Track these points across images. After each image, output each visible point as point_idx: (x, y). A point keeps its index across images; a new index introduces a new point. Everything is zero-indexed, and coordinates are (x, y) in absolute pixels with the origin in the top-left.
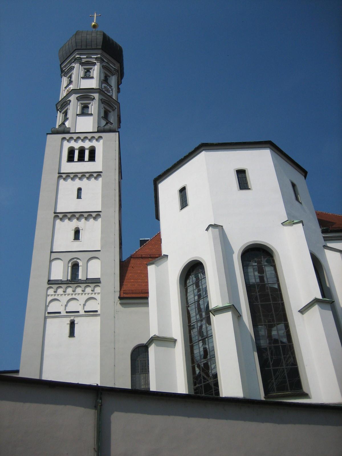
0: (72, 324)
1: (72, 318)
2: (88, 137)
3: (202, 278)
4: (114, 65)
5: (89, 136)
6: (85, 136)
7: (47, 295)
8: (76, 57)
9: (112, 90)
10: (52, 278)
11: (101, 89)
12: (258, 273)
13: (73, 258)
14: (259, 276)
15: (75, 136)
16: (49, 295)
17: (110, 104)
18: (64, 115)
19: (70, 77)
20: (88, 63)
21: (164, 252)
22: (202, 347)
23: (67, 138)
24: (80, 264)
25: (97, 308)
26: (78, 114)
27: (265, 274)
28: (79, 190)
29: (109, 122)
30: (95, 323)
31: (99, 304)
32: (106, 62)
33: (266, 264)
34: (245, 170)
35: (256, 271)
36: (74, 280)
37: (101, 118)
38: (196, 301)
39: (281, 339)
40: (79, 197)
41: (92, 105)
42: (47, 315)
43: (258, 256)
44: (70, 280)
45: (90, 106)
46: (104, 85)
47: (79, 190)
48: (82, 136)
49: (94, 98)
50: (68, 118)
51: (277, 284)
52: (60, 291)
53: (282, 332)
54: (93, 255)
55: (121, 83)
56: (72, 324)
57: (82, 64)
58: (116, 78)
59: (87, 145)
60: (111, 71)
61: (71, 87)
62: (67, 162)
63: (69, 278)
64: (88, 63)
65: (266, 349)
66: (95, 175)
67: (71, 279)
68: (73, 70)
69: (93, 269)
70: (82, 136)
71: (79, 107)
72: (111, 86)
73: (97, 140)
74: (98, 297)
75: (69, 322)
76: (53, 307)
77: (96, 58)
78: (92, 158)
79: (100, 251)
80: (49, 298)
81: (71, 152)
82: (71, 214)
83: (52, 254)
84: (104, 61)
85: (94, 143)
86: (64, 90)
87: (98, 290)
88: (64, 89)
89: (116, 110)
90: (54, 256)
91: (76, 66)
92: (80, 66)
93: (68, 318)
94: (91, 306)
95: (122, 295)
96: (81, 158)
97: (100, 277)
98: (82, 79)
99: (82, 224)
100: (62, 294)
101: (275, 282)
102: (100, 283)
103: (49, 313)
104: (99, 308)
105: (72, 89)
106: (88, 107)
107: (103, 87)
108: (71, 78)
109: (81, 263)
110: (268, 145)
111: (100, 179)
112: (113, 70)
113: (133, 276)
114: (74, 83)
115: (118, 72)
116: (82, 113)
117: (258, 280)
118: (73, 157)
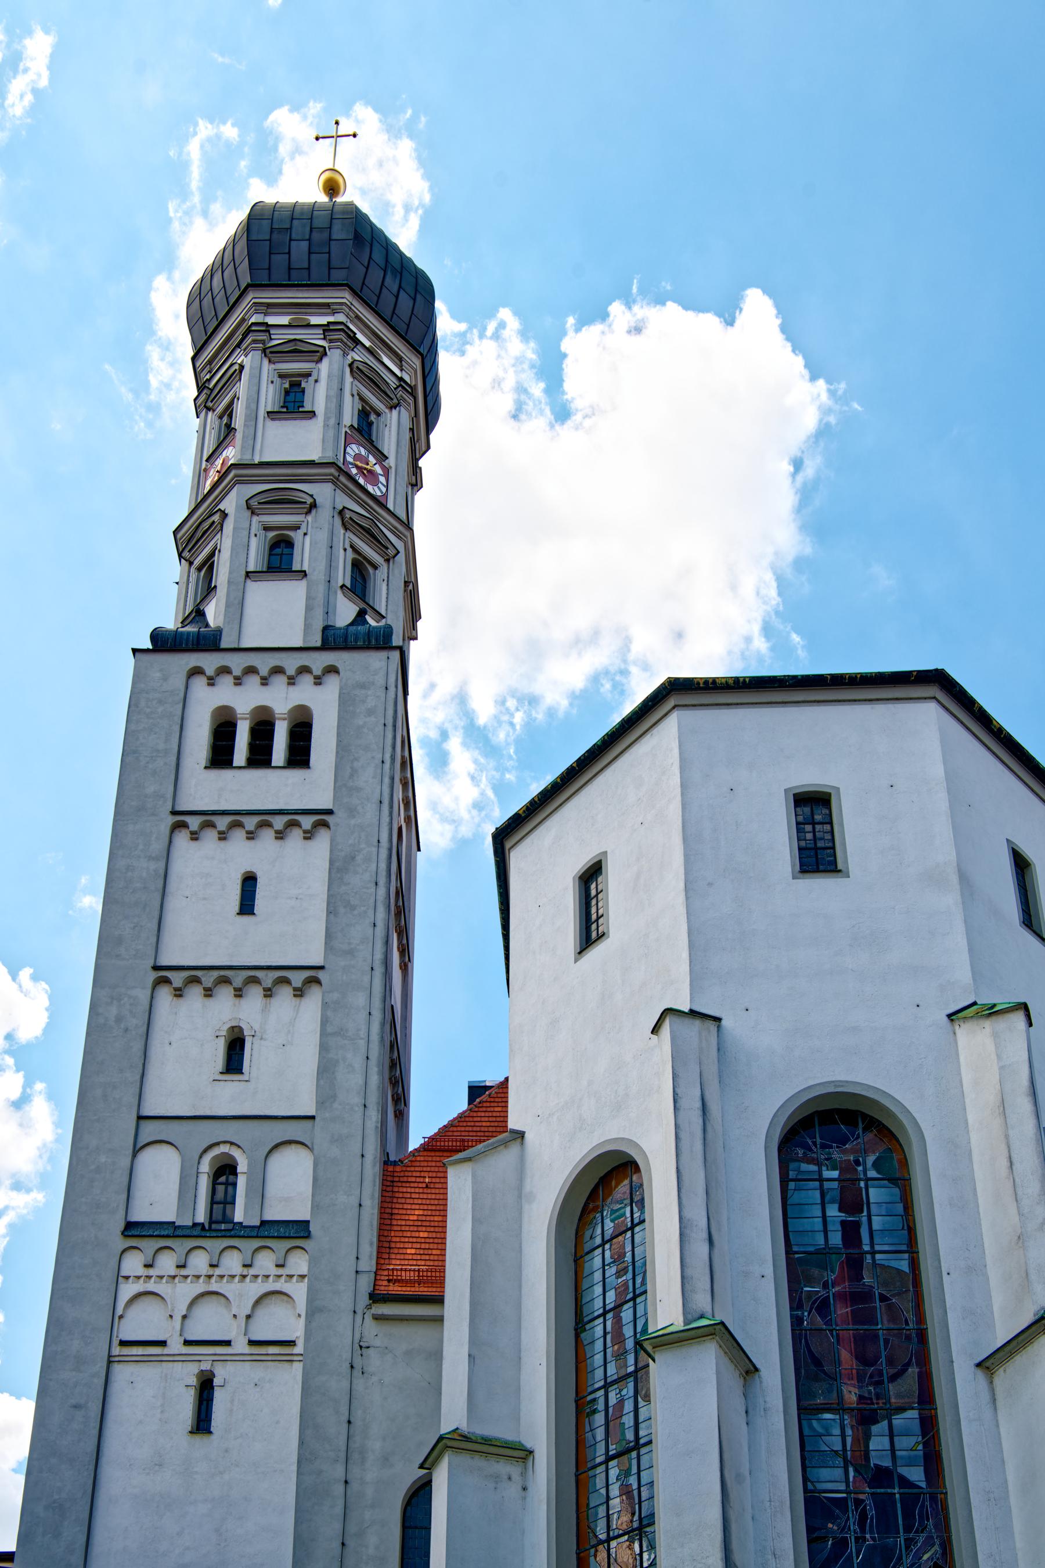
0: (206, 1387)
1: (206, 1366)
2: (286, 668)
3: (636, 1221)
4: (399, 360)
5: (291, 663)
6: (273, 664)
7: (120, 1278)
8: (253, 320)
9: (386, 472)
10: (140, 1215)
11: (341, 465)
12: (840, 1210)
13: (218, 1144)
14: (843, 1223)
15: (237, 663)
16: (127, 1278)
17: (375, 531)
18: (203, 573)
19: (229, 411)
20: (296, 350)
21: (514, 1122)
22: (619, 1483)
23: (210, 671)
24: (242, 1168)
25: (295, 1329)
26: (251, 568)
27: (865, 1213)
28: (249, 881)
29: (369, 610)
30: (287, 1382)
31: (299, 1315)
32: (367, 349)
33: (872, 1174)
34: (830, 794)
35: (832, 1202)
36: (219, 1225)
37: (339, 592)
38: (608, 1308)
39: (903, 1471)
40: (247, 907)
41: (305, 534)
42: (116, 1350)
43: (842, 1141)
44: (203, 1224)
45: (297, 536)
46: (354, 449)
47: (249, 881)
48: (264, 663)
49: (314, 505)
50: (215, 587)
51: (906, 1256)
52: (167, 1263)
53: (910, 1443)
54: (289, 1130)
55: (428, 448)
56: (206, 1387)
57: (270, 353)
58: (407, 424)
59: (280, 699)
60: (384, 387)
61: (231, 454)
62: (206, 768)
63: (201, 1217)
64: (296, 350)
65: (841, 1503)
66: (307, 822)
67: (211, 1222)
68: (240, 380)
69: (288, 1186)
70: (264, 663)
71: (254, 542)
72: (381, 457)
73: (318, 681)
74: (299, 1291)
75: (193, 1381)
76: (143, 1322)
77: (326, 329)
78: (299, 756)
79: (313, 1118)
80: (128, 1290)
81: (223, 731)
82: (216, 974)
83: (143, 1123)
84: (357, 342)
85: (304, 694)
86: (205, 470)
87: (299, 1263)
88: (203, 466)
89: (401, 558)
90: (150, 1131)
91: (249, 360)
92: (266, 362)
93: (190, 1364)
94: (284, 1322)
95: (382, 1288)
96: (259, 757)
97: (308, 1218)
98: (270, 423)
99: (248, 1011)
100: (173, 1274)
101: (904, 1248)
102: (308, 1236)
103: (123, 1343)
104: (298, 1334)
105: (231, 462)
106: (290, 544)
107: (349, 459)
108: (230, 416)
109: (246, 1162)
110: (934, 691)
111: (323, 838)
112: (392, 382)
113: (428, 1218)
114: (239, 435)
115: (411, 394)
116: (269, 568)
117: (836, 1239)
118: (230, 750)
